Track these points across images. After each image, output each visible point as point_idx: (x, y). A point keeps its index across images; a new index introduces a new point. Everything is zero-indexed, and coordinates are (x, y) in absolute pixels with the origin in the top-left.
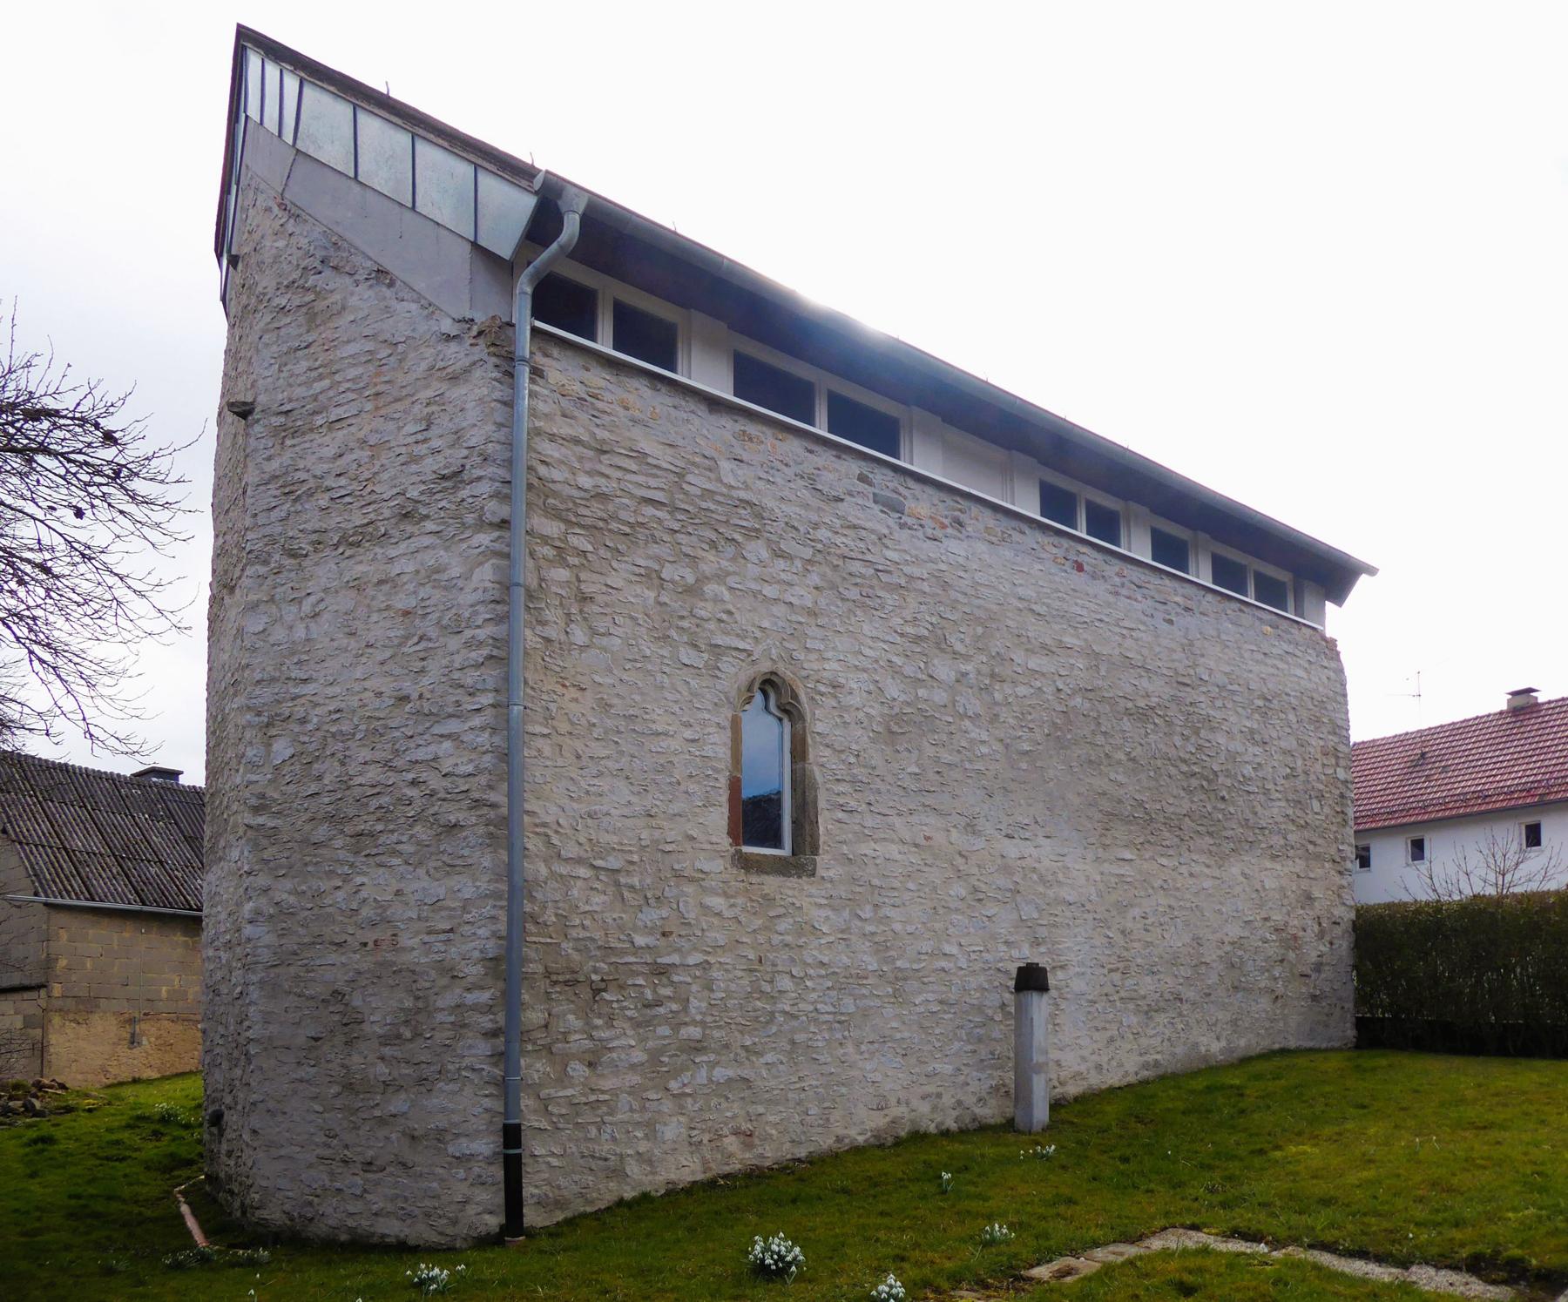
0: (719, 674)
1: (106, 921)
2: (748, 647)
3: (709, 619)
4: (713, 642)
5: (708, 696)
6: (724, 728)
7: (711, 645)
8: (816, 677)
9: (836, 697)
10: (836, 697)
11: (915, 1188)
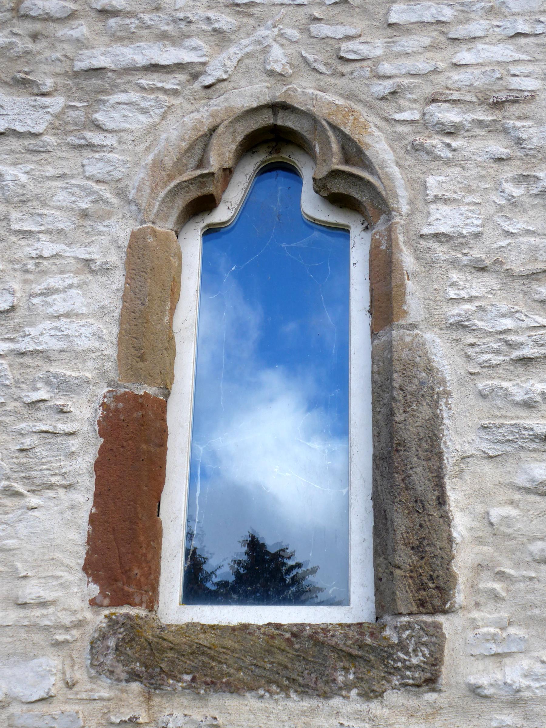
0: (96, 138)
1: (7, 341)
2: (187, 57)
3: (72, 15)
4: (80, 65)
5: (62, 197)
6: (105, 270)
7: (76, 74)
8: (429, 91)
9: (505, 130)
10: (505, 130)
11: (203, 101)
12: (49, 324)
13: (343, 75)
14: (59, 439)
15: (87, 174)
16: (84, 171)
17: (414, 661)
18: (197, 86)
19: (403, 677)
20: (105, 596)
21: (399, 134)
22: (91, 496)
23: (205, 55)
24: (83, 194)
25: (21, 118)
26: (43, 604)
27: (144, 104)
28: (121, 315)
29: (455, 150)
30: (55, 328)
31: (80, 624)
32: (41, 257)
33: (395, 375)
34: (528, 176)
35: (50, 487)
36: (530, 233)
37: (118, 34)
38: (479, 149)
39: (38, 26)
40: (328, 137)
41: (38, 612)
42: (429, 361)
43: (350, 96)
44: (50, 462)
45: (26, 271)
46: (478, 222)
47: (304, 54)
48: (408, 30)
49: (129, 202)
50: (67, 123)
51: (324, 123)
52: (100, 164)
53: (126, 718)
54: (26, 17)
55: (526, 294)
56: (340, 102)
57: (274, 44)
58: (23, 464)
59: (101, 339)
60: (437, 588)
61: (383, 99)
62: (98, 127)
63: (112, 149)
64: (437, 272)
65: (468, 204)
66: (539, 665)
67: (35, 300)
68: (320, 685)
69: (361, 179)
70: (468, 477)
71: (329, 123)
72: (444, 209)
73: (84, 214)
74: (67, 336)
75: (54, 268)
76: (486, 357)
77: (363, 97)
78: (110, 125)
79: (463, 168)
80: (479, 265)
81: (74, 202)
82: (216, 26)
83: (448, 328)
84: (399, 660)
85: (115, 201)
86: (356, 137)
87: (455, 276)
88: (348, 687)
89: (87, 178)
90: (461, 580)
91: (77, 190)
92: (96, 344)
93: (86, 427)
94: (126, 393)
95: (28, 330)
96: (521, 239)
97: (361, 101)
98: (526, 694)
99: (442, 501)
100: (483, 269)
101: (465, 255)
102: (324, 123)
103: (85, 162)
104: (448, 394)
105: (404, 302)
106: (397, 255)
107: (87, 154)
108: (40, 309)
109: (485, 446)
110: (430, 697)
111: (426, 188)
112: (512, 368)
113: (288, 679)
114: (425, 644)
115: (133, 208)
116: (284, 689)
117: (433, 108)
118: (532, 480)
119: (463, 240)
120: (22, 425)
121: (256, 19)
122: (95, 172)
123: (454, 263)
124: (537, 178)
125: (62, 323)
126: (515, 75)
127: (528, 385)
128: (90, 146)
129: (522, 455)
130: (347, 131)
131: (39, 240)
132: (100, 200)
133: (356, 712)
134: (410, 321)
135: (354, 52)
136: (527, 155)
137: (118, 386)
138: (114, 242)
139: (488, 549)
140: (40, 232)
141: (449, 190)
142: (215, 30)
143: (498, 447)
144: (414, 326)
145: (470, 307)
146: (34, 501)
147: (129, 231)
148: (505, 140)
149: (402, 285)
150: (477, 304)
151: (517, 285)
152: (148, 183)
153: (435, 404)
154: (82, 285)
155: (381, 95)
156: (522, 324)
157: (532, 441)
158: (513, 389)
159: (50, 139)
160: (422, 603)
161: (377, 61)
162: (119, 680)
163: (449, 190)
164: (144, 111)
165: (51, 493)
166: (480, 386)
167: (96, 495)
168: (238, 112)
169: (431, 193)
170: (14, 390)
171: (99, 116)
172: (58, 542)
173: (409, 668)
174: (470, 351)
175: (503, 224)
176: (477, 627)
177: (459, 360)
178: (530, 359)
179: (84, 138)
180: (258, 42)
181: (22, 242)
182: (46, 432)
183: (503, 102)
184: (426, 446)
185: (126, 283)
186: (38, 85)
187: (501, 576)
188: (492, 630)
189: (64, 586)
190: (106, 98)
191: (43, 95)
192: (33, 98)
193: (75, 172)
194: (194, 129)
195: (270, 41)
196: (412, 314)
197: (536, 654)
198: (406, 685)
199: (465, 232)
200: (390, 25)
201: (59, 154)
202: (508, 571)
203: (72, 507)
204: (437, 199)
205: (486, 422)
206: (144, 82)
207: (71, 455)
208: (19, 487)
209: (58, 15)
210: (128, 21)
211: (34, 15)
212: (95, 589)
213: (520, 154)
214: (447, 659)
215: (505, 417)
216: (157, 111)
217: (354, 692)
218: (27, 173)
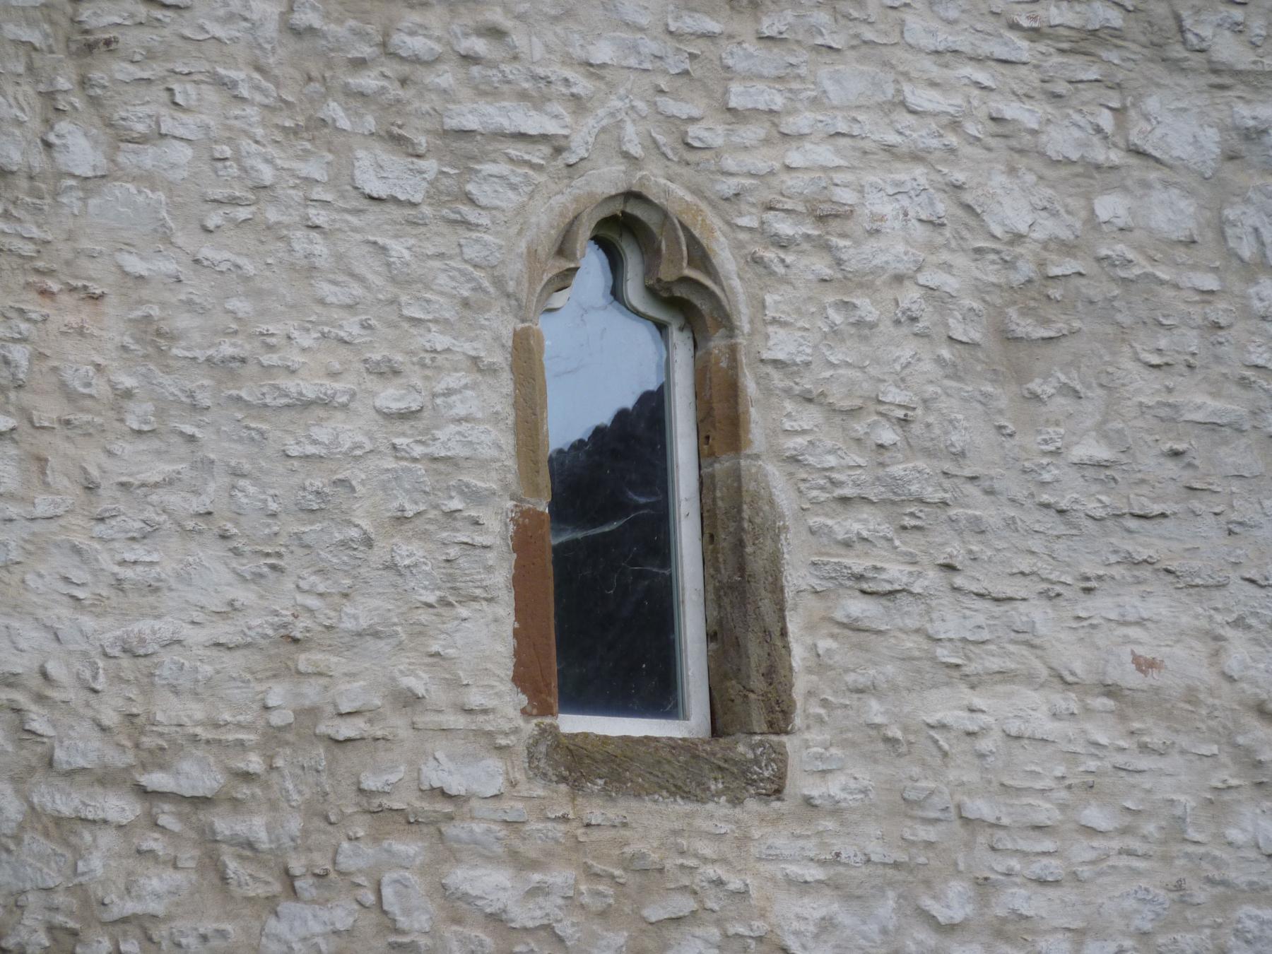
2: (552, 128)
3: (438, 60)
4: (452, 123)
5: (443, 279)
6: (492, 370)
7: (446, 132)
9: (827, 248)
10: (827, 248)
12: (453, 428)
13: (688, 164)
14: (477, 552)
15: (466, 257)
16: (462, 253)
17: (766, 774)
18: (560, 162)
19: (758, 788)
20: (534, 707)
21: (740, 241)
22: (511, 610)
23: (567, 127)
24: (463, 279)
25: (401, 182)
26: (485, 711)
27: (514, 180)
28: (516, 424)
29: (787, 267)
30: (459, 433)
31: (516, 731)
32: (435, 351)
33: (745, 507)
34: (847, 303)
35: (475, 599)
36: (848, 365)
37: (482, 87)
38: (806, 266)
39: (406, 69)
40: (677, 238)
41: (481, 718)
42: (771, 494)
43: (697, 191)
44: (471, 574)
45: (424, 366)
46: (809, 351)
47: (654, 135)
48: (745, 117)
49: (508, 296)
50: (441, 192)
51: (676, 221)
52: (477, 247)
53: (560, 814)
54: (394, 55)
55: (844, 429)
56: (689, 197)
57: (626, 118)
58: (450, 575)
59: (500, 447)
60: (782, 711)
61: (727, 199)
62: (471, 201)
63: (487, 230)
64: (774, 400)
65: (800, 329)
66: (852, 781)
67: (439, 401)
68: (698, 792)
69: (705, 288)
70: (800, 610)
71: (681, 223)
72: (782, 333)
73: (466, 303)
74: (471, 443)
75: (447, 365)
76: (815, 493)
77: (708, 194)
78: (483, 201)
79: (795, 288)
80: (808, 396)
81: (455, 288)
82: (574, 90)
83: (784, 460)
84: (756, 773)
85: (492, 290)
86: (704, 242)
87: (789, 406)
88: (719, 794)
89: (466, 261)
90: (799, 705)
91: (456, 274)
92: (495, 453)
93: (498, 541)
94: (529, 509)
95: (438, 433)
96: (841, 371)
97: (706, 198)
98: (843, 805)
99: (784, 633)
100: (810, 400)
101: (797, 384)
102: (676, 221)
103: (463, 241)
104: (786, 528)
105: (748, 431)
106: (742, 380)
107: (461, 231)
108: (443, 411)
109: (815, 582)
110: (776, 805)
111: (764, 307)
112: (833, 505)
113: (675, 786)
114: (773, 760)
115: (513, 302)
116: (672, 794)
117: (770, 216)
118: (848, 616)
119: (795, 368)
120: (445, 534)
121: (607, 84)
122: (473, 256)
123: (788, 392)
124: (855, 306)
125: (464, 427)
126: (837, 185)
127: (847, 524)
128: (466, 224)
129: (841, 591)
130: (697, 233)
131: (429, 331)
132: (479, 288)
133: (726, 816)
134: (755, 451)
135: (700, 139)
136: (845, 278)
137: (521, 500)
138: (497, 338)
139: (814, 678)
140: (429, 321)
141: (783, 312)
142: (573, 95)
143: (823, 583)
144: (757, 457)
145: (801, 441)
146: (463, 611)
147: (510, 328)
148: (828, 259)
149: (747, 412)
150: (809, 438)
151: (837, 419)
152: (526, 276)
153: (776, 539)
154: (474, 386)
155: (727, 195)
156: (843, 462)
157: (849, 579)
158: (836, 528)
159: (427, 210)
160: (771, 724)
161: (718, 153)
162: (550, 781)
163: (783, 312)
164: (514, 187)
165: (476, 605)
166: (811, 522)
167: (516, 610)
168: (600, 200)
169: (770, 313)
170: (432, 497)
171: (470, 187)
172: (487, 653)
173: (762, 780)
174: (803, 486)
175: (827, 353)
176: (808, 747)
177: (794, 495)
178: (849, 499)
179: (459, 213)
180: (612, 115)
181: (414, 331)
182: (466, 543)
183: (827, 216)
184: (770, 579)
185: (515, 388)
186: (413, 144)
187: (825, 703)
188: (820, 750)
189: (499, 695)
190: (477, 167)
191: (419, 156)
192: (410, 159)
193: (453, 252)
194: (562, 215)
195: (622, 115)
196: (757, 443)
197: (849, 772)
198: (761, 794)
199: (798, 360)
200: (729, 110)
201: (435, 229)
202: (830, 698)
203: (496, 620)
204: (774, 321)
205: (815, 559)
206: (513, 152)
207: (489, 569)
208: (451, 599)
209: (425, 58)
210: (490, 72)
211: (404, 55)
212: (523, 700)
213: (839, 276)
214: (789, 774)
215: (828, 554)
216: (526, 189)
217: (723, 799)
218: (408, 248)
